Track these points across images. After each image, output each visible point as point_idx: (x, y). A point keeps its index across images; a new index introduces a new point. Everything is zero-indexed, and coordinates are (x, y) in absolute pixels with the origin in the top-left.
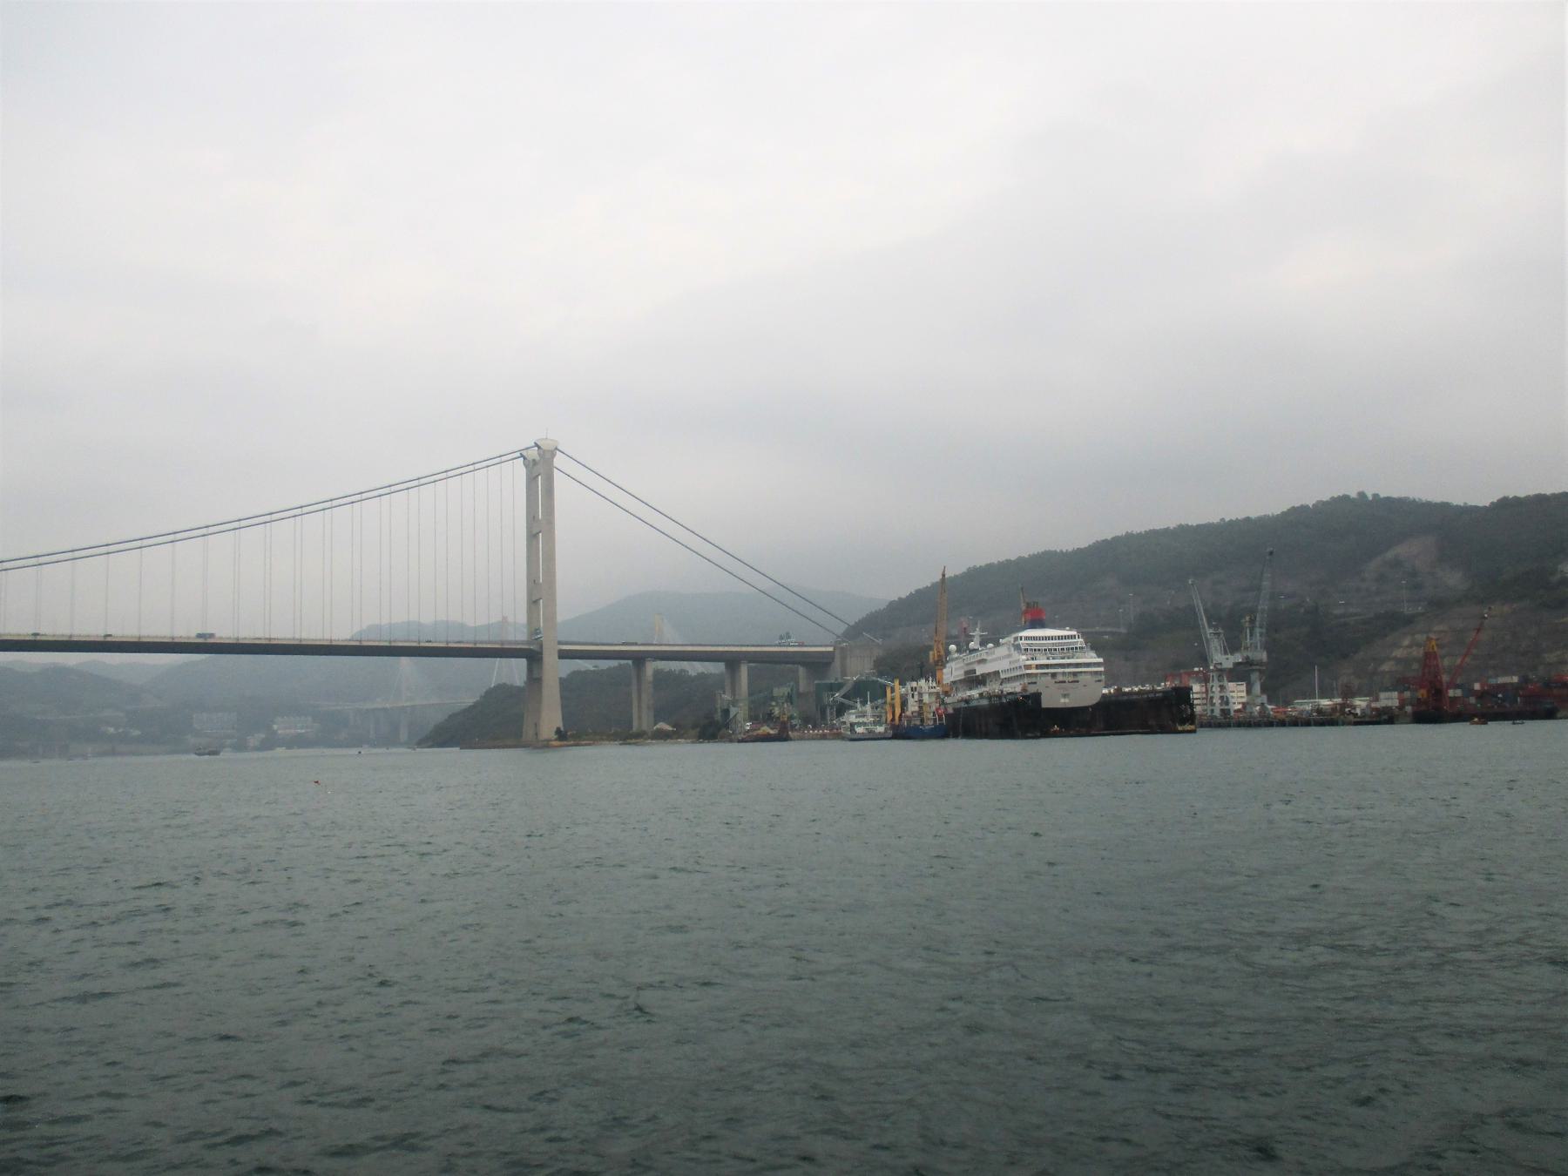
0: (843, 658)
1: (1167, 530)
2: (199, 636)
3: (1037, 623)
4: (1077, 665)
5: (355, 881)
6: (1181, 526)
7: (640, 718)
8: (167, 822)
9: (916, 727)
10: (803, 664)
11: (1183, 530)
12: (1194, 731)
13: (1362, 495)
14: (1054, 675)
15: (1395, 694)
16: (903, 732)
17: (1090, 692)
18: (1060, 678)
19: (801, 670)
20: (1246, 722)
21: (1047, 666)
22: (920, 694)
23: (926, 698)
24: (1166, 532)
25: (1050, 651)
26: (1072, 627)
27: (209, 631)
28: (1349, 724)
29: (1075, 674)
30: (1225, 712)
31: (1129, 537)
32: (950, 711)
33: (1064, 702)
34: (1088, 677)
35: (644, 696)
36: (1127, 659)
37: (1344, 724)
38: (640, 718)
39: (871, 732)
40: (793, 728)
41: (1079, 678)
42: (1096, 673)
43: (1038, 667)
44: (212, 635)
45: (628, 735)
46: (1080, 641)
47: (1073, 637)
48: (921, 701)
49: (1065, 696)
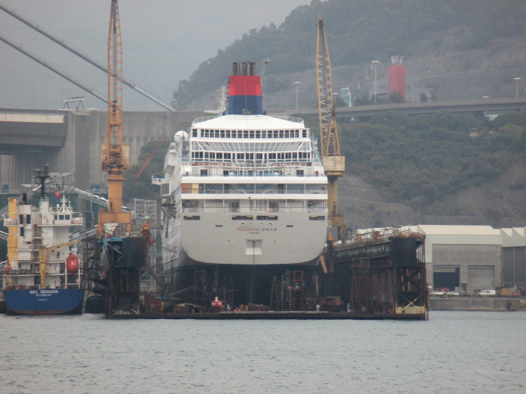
2: (19, 318)
3: (245, 102)
4: (281, 188)
13: (245, 36)
14: (235, 204)
18: (244, 210)
21: (228, 188)
22: (37, 229)
23: (48, 238)
25: (252, 160)
26: (294, 117)
27: (18, 320)
29: (274, 204)
32: (456, 288)
33: (252, 255)
34: (303, 211)
41: (284, 212)
42: (311, 203)
44: (17, 318)
46: (305, 143)
47: (293, 133)
48: (37, 242)
49: (254, 243)
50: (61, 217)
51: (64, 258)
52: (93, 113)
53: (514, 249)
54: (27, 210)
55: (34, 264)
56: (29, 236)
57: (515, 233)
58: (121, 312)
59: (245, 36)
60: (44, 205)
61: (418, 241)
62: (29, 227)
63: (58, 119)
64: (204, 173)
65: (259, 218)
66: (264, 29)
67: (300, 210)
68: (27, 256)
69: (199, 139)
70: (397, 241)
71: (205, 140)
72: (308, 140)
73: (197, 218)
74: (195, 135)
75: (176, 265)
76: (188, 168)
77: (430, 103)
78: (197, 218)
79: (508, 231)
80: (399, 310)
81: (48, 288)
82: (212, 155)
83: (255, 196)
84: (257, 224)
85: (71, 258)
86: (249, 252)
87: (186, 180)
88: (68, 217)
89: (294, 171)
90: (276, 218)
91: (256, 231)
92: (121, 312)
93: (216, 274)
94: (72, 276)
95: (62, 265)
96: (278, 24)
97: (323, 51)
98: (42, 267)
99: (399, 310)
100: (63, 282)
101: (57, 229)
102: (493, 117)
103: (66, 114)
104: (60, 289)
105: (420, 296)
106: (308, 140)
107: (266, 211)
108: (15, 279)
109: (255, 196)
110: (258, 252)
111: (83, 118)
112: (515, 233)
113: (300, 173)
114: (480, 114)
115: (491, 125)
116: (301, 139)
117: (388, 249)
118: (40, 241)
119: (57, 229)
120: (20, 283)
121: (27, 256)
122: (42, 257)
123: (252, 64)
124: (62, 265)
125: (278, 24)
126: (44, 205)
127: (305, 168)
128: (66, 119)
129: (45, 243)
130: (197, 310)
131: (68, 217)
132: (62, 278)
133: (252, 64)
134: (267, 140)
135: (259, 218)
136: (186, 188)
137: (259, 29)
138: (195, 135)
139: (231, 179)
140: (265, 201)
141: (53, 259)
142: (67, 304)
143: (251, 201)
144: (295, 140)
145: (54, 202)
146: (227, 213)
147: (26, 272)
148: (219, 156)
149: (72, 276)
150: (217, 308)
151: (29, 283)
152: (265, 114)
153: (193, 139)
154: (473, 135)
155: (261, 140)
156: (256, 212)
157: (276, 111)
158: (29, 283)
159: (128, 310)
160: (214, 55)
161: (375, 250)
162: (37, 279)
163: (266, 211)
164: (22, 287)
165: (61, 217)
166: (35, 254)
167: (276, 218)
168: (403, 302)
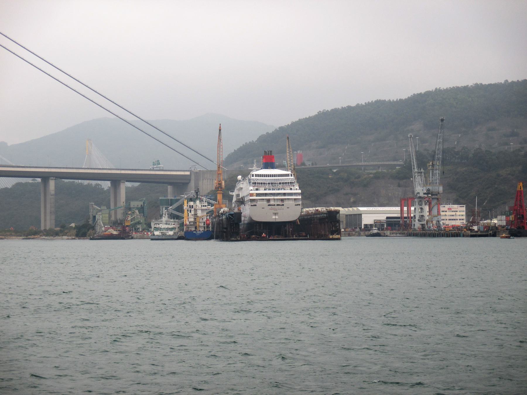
0: (197, 180)
1: (466, 88)
3: (269, 165)
4: (284, 194)
5: (312, 391)
6: (476, 84)
7: (45, 220)
8: (507, 334)
9: (192, 232)
10: (170, 184)
11: (478, 87)
12: (338, 239)
14: (268, 200)
15: (504, 217)
16: (188, 235)
17: (291, 212)
18: (272, 203)
19: (170, 188)
20: (455, 233)
21: (266, 194)
22: (196, 210)
23: (199, 213)
24: (465, 89)
26: (287, 170)
28: (468, 236)
29: (282, 200)
30: (439, 226)
31: (438, 92)
33: (274, 218)
34: (292, 203)
35: (48, 206)
36: (399, 186)
37: (464, 236)
38: (45, 220)
39: (163, 234)
40: (137, 230)
41: (286, 203)
42: (295, 199)
43: (258, 195)
45: (31, 232)
46: (292, 178)
47: (287, 175)
48: (196, 214)
49: (275, 214)
50: (204, 206)
51: (205, 220)
52: (200, 171)
53: (47, 222)
54: (192, 203)
55: (195, 222)
56: (193, 213)
57: (353, 209)
58: (233, 239)
59: (243, 145)
60: (198, 202)
61: (338, 212)
62: (193, 209)
63: (188, 173)
64: (257, 190)
65: (277, 205)
66: (250, 142)
67: (291, 202)
68: (192, 220)
69: (254, 178)
70: (330, 213)
71: (256, 178)
72: (292, 177)
73: (256, 205)
74: (253, 176)
75: (246, 222)
76: (251, 188)
77: (314, 166)
78: (256, 205)
79: (346, 209)
80: (331, 237)
81: (200, 231)
82: (259, 183)
83: (276, 197)
84: (276, 207)
85: (207, 220)
86: (274, 217)
87: (251, 192)
88: (206, 206)
89: (289, 189)
90: (283, 205)
91: (276, 210)
92: (233, 239)
93: (262, 225)
94: (208, 227)
95: (204, 223)
96: (254, 141)
97: (289, 147)
98: (198, 223)
99: (331, 237)
100: (205, 228)
101: (202, 210)
102: (335, 171)
103: (191, 171)
104: (204, 231)
105: (338, 232)
106: (292, 177)
107: (280, 203)
108: (188, 228)
109: (276, 197)
110: (277, 217)
111: (197, 172)
112: (353, 209)
113: (291, 189)
114: (331, 170)
115: (334, 173)
116: (290, 177)
117: (325, 215)
118: (197, 214)
119: (202, 210)
120: (190, 229)
121: (192, 220)
122: (197, 220)
123: (271, 151)
124: (204, 223)
125: (254, 141)
126: (198, 202)
127: (292, 187)
128: (191, 173)
129: (198, 215)
130: (258, 238)
131: (206, 206)
132: (204, 227)
133: (271, 151)
134: (278, 178)
135: (277, 205)
136: (252, 195)
137: (248, 142)
138: (253, 176)
139: (267, 192)
140: (279, 199)
141: (201, 220)
142: (207, 236)
143: (274, 199)
144: (288, 177)
145: (201, 200)
146: (265, 202)
147: (192, 225)
148: (262, 183)
149: (208, 227)
150: (264, 237)
151: (193, 229)
152: (276, 168)
153: (252, 178)
154: (330, 177)
155: (276, 178)
156: (276, 203)
157: (281, 167)
158: (193, 229)
159: (236, 238)
160: (233, 151)
161: (318, 216)
162: (196, 228)
163: (280, 203)
164: (191, 230)
165: (204, 206)
166: (195, 219)
167: (283, 205)
168: (332, 234)
